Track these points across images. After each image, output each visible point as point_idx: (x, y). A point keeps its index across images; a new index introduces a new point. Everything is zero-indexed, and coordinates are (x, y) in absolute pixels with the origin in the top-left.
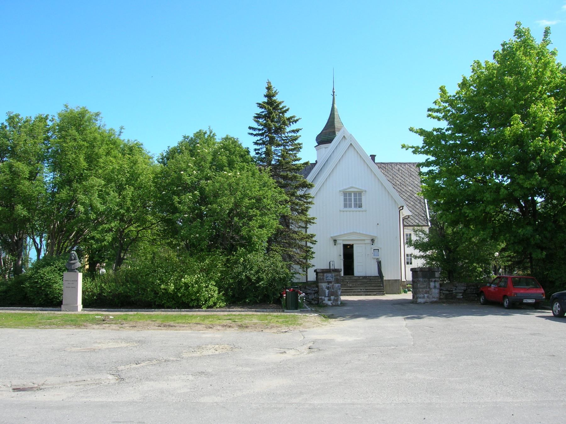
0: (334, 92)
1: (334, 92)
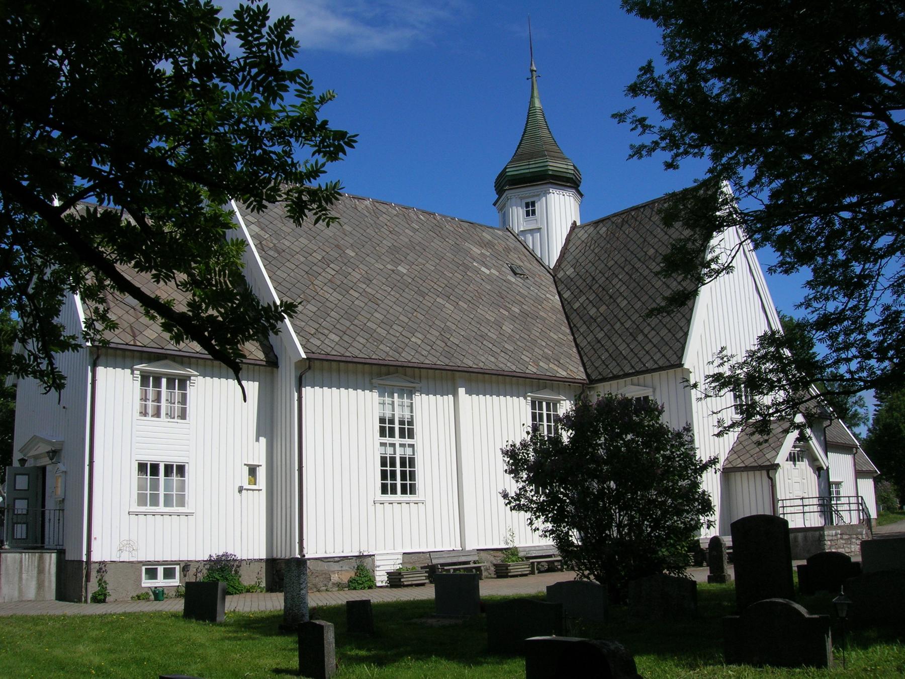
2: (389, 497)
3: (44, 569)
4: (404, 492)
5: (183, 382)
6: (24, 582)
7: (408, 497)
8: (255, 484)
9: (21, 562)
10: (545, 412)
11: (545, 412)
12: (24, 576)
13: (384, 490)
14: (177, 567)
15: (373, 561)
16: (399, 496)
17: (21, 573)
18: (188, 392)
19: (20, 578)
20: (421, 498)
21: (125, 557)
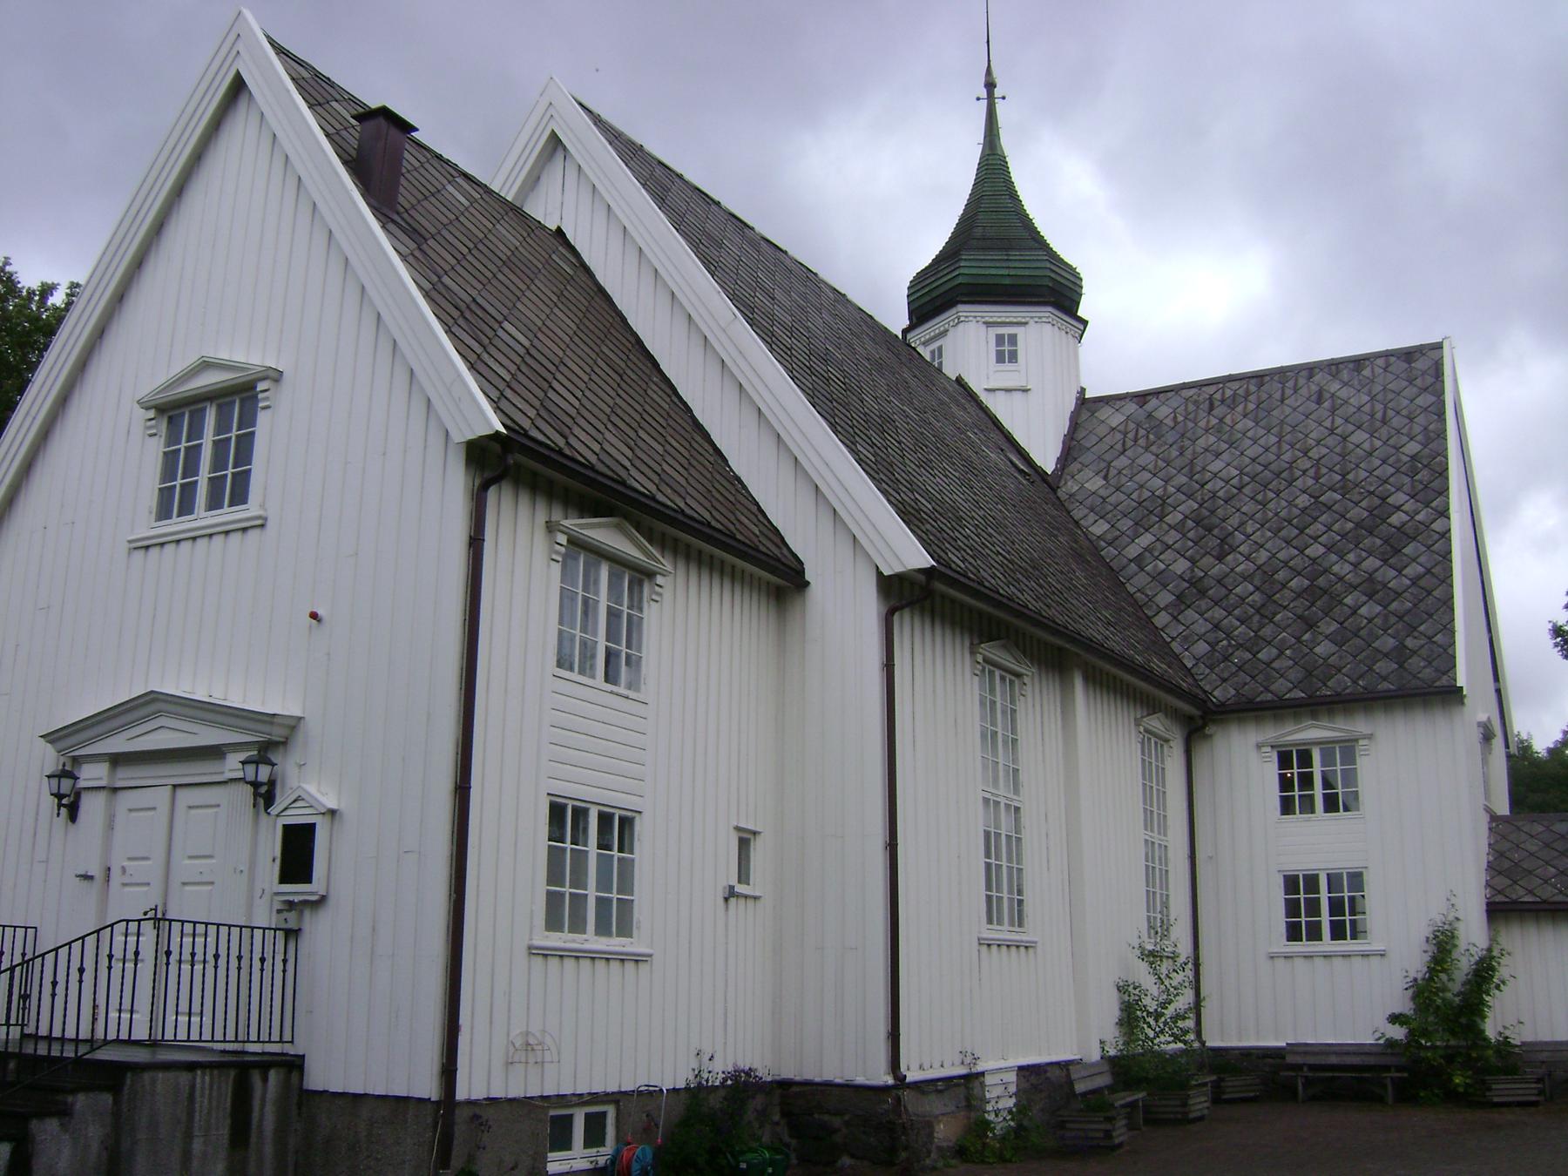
0: (990, 85)
1: (990, 85)
2: (1297, 947)
3: (248, 1123)
4: (1338, 932)
5: (642, 575)
6: (195, 1164)
7: (1347, 945)
8: (625, 930)
9: (193, 1087)
10: (592, 892)
11: (592, 892)
12: (197, 1146)
13: (1293, 933)
14: (611, 1111)
15: (982, 1084)
16: (1327, 944)
17: (188, 1136)
18: (645, 615)
19: (187, 1156)
20: (1377, 946)
21: (532, 1086)
